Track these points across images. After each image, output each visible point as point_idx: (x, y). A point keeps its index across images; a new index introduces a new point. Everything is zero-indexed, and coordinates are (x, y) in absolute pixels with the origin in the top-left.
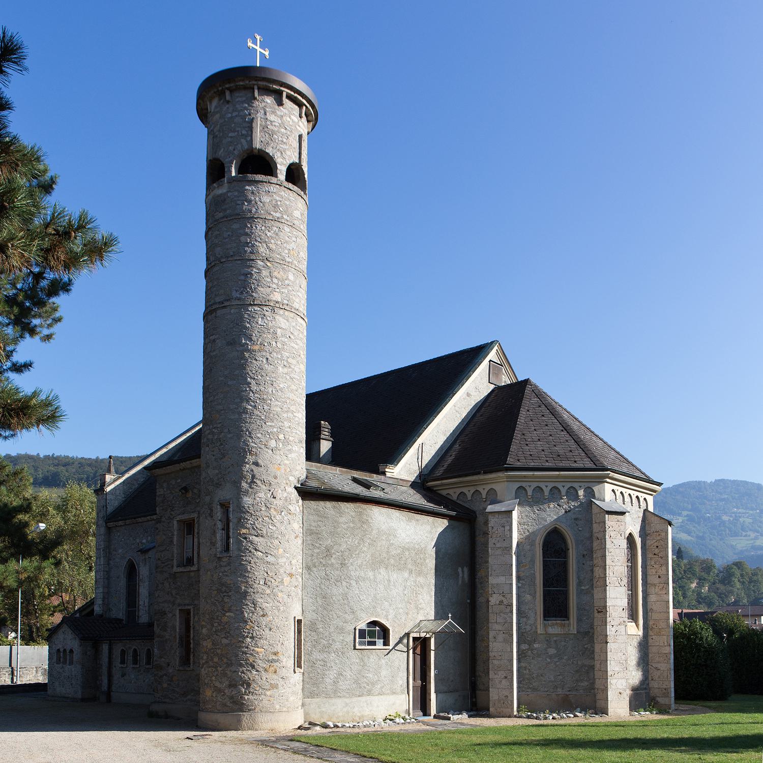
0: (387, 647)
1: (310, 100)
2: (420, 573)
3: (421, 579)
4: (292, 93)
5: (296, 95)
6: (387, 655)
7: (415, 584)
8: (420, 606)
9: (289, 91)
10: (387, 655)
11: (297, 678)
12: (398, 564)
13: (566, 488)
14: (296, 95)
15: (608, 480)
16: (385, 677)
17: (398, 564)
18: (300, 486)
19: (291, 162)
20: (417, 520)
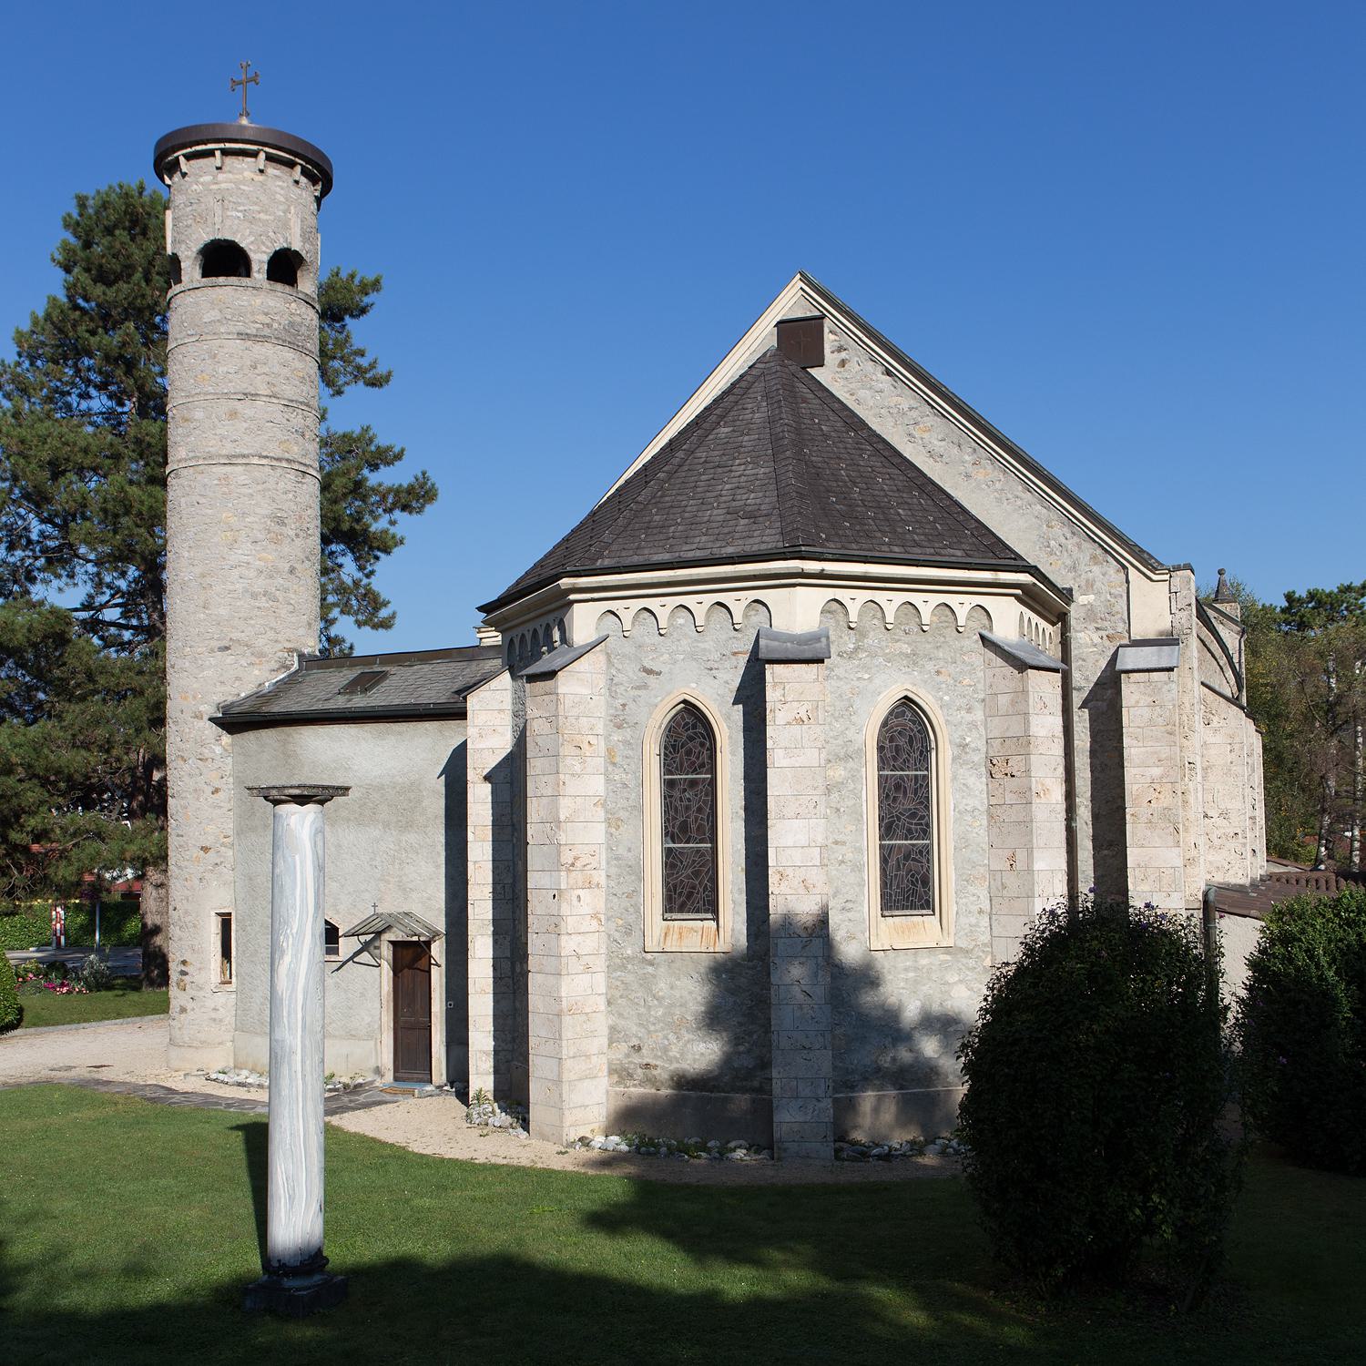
0: (333, 958)
1: (291, 150)
2: (408, 826)
3: (411, 838)
4: (189, 150)
5: (194, 149)
6: (337, 970)
7: (397, 847)
8: (410, 886)
9: (184, 151)
10: (337, 970)
11: (225, 1002)
12: (357, 816)
13: (967, 607)
14: (194, 149)
15: (572, 597)
16: (333, 1008)
17: (357, 816)
18: (221, 715)
19: (271, 252)
20: (400, 733)
